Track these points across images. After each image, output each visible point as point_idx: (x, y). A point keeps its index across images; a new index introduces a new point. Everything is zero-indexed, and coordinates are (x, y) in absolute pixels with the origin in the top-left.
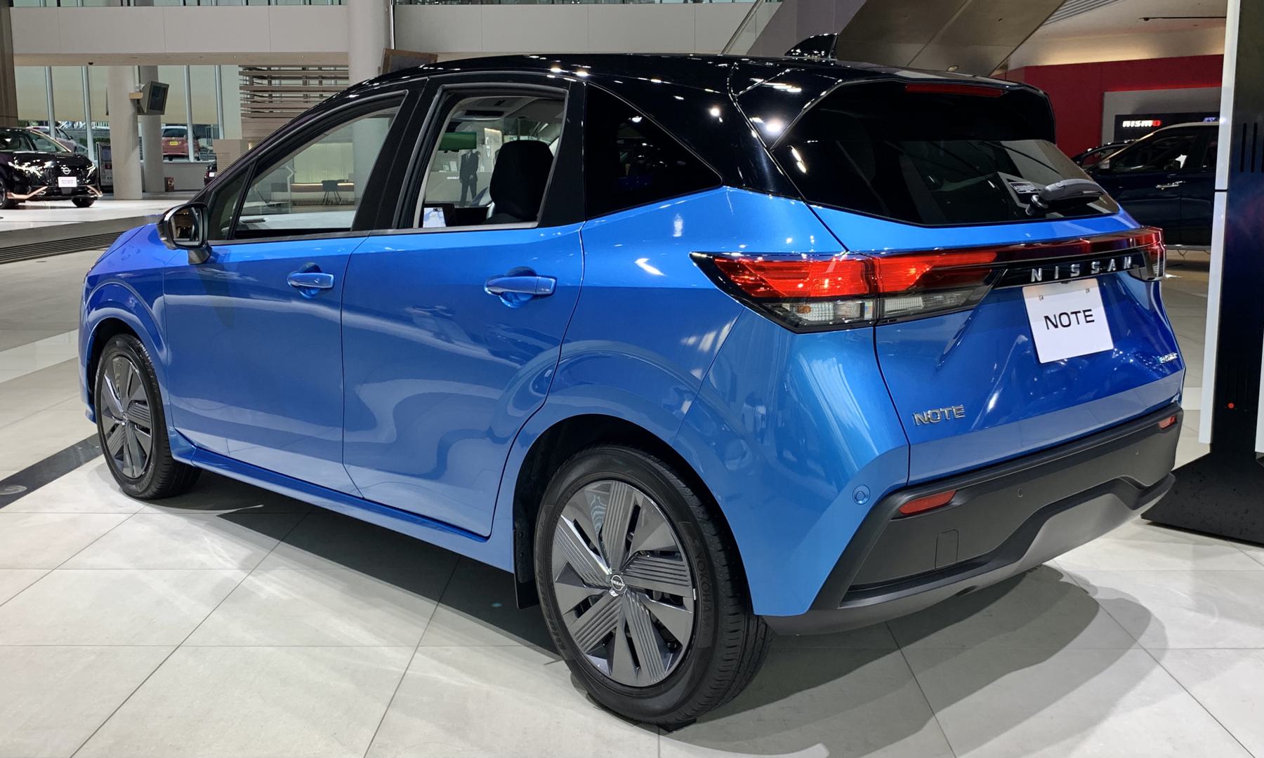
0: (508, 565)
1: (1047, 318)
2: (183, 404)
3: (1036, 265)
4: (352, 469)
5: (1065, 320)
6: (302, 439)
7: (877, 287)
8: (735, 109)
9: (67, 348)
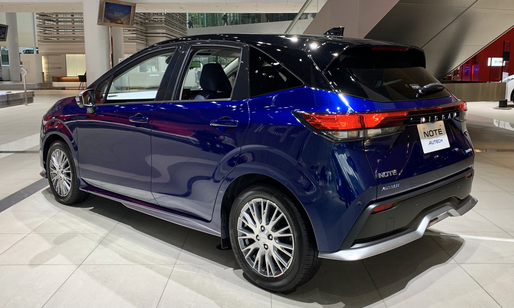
0: (218, 233)
1: (424, 133)
2: (82, 166)
3: (422, 116)
4: (153, 193)
5: (431, 133)
6: (127, 179)
7: (364, 125)
8: (402, 174)
9: (35, 141)
